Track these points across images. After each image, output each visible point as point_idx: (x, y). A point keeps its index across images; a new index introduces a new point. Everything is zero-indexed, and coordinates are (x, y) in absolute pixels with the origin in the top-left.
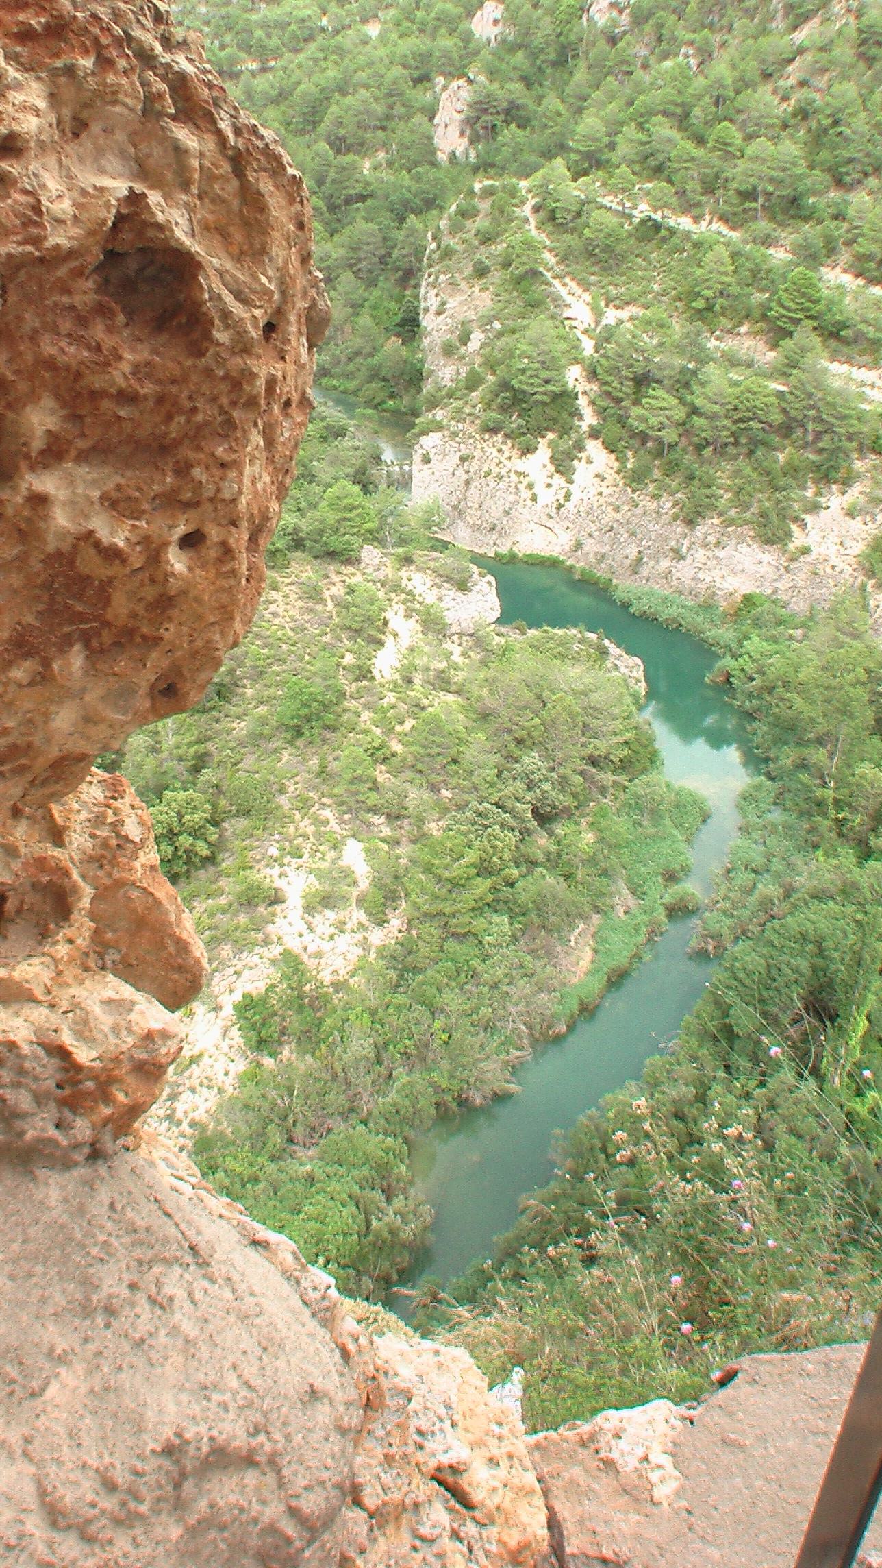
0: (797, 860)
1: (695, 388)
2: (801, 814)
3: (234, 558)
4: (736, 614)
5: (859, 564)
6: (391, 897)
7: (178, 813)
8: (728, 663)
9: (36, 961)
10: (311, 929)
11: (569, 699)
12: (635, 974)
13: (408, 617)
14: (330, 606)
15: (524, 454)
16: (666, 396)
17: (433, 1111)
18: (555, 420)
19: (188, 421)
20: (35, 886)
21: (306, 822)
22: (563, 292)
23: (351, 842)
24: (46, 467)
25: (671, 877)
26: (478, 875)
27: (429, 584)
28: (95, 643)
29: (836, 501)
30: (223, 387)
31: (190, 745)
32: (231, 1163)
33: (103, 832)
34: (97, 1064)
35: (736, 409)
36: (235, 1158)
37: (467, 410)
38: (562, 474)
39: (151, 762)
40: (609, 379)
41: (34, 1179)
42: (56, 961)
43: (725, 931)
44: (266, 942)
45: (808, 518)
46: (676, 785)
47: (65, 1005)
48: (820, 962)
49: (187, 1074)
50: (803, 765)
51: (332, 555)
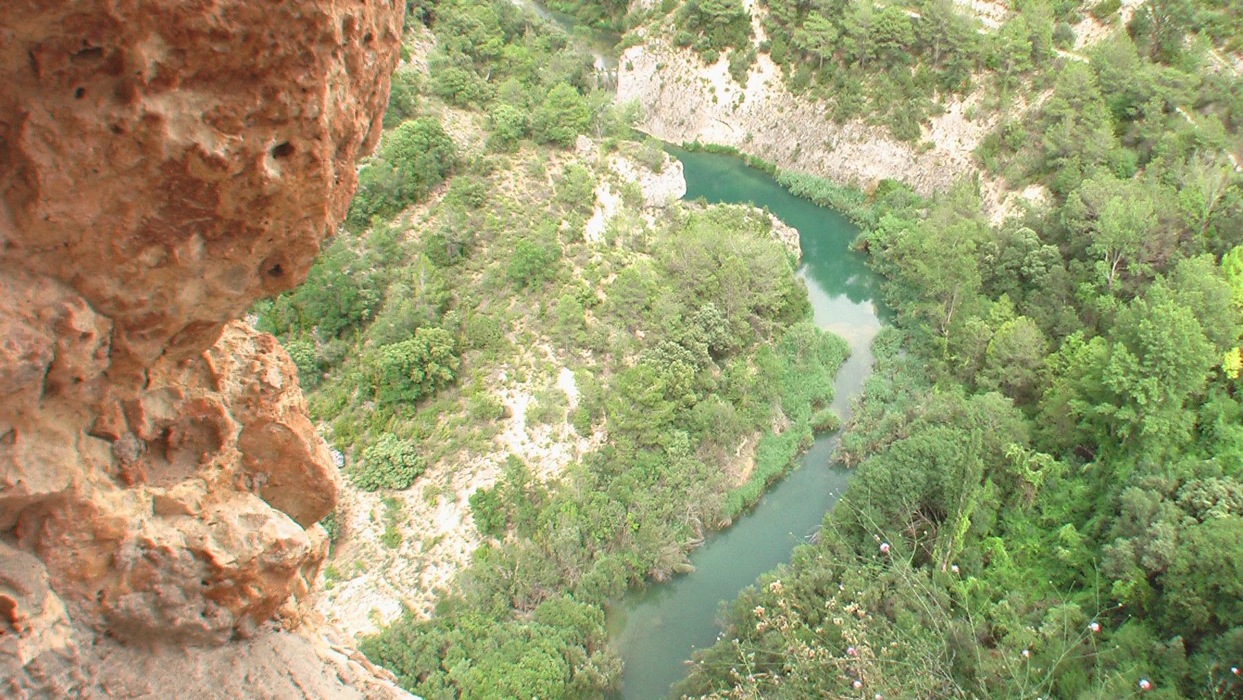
0: (917, 392)
1: (846, 14)
2: (922, 356)
3: (319, 166)
4: (874, 196)
5: (974, 157)
6: (595, 415)
7: (428, 345)
8: (867, 235)
9: (190, 482)
10: (531, 439)
11: (740, 261)
12: (787, 480)
13: (612, 192)
14: (551, 183)
15: (707, 64)
16: (821, 19)
17: (625, 584)
18: (733, 38)
19: (272, 54)
20: (194, 422)
21: (529, 354)
23: (565, 371)
24: (158, 92)
25: (817, 404)
26: (664, 398)
27: (630, 166)
28: (209, 233)
29: (956, 107)
30: (300, 27)
31: (438, 291)
32: (465, 622)
33: (251, 380)
34: (234, 566)
35: (878, 31)
36: (469, 618)
37: (663, 28)
38: (738, 81)
39: (407, 304)
40: (777, 5)
41: (185, 656)
42: (208, 483)
43: (859, 447)
44: (496, 449)
45: (934, 120)
46: (823, 331)
47: (211, 518)
48: (933, 473)
49: (431, 551)
50: (924, 317)
51: (553, 142)
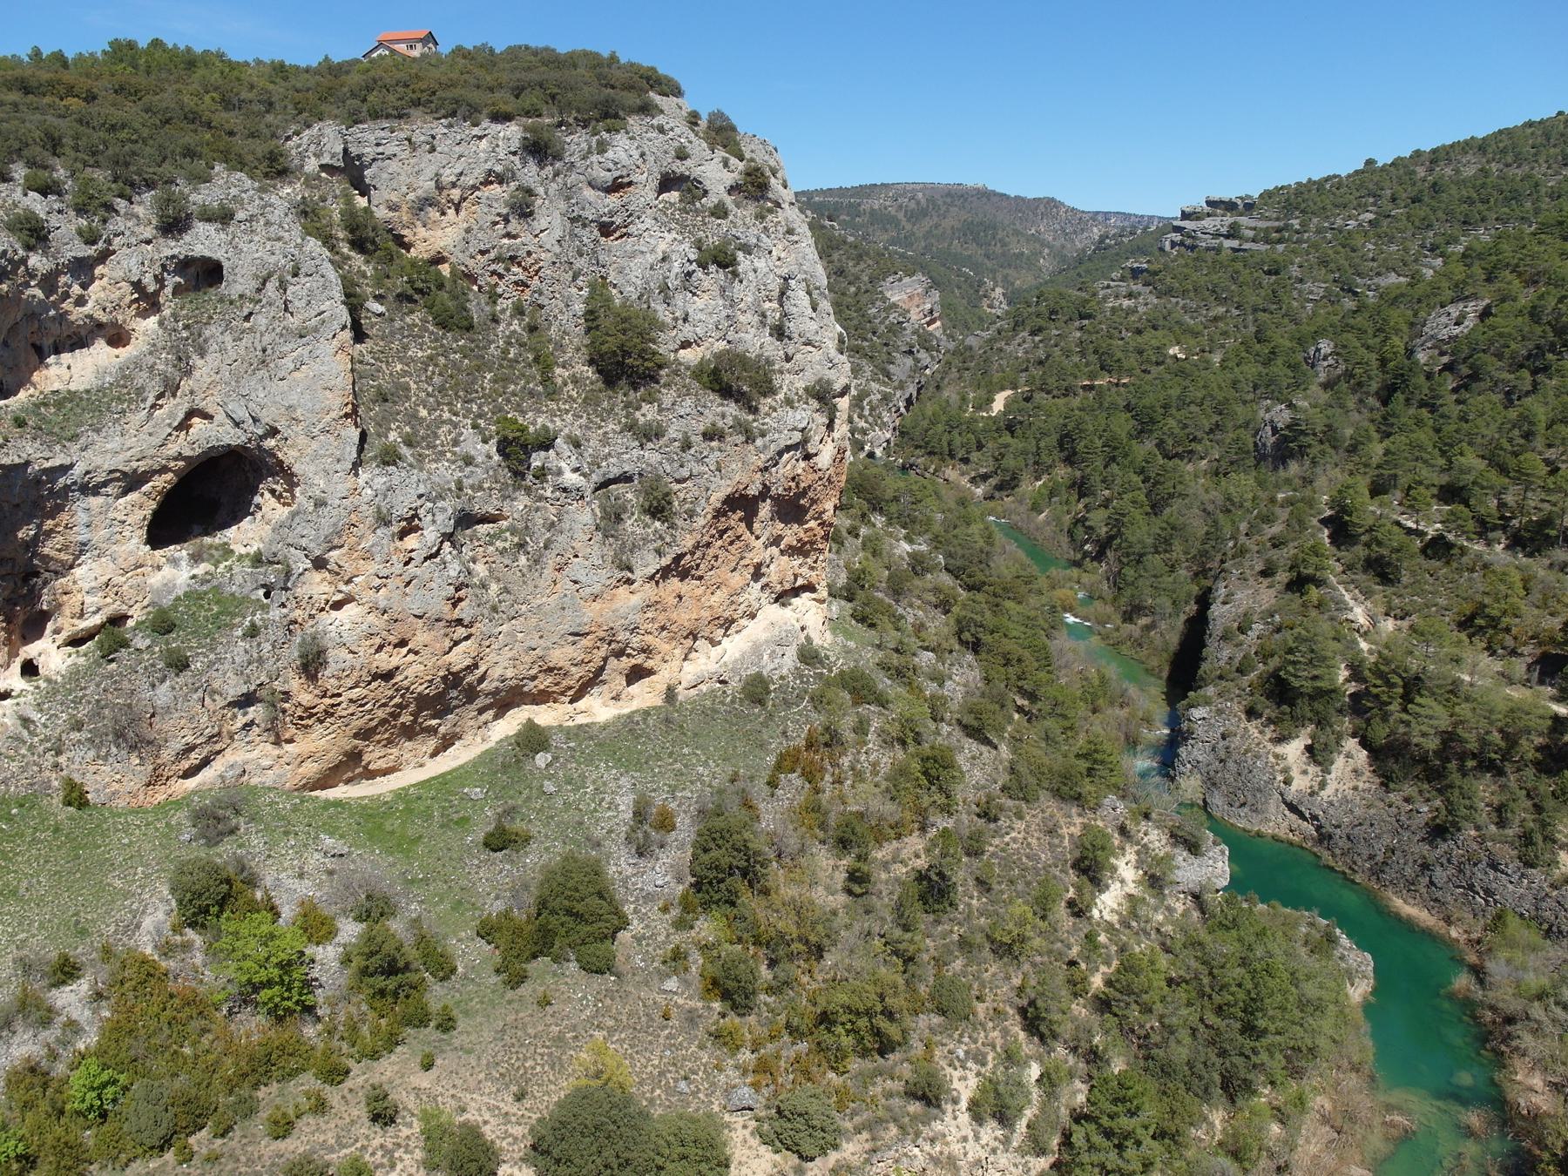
16: (1434, 704)
22: (1347, 597)
